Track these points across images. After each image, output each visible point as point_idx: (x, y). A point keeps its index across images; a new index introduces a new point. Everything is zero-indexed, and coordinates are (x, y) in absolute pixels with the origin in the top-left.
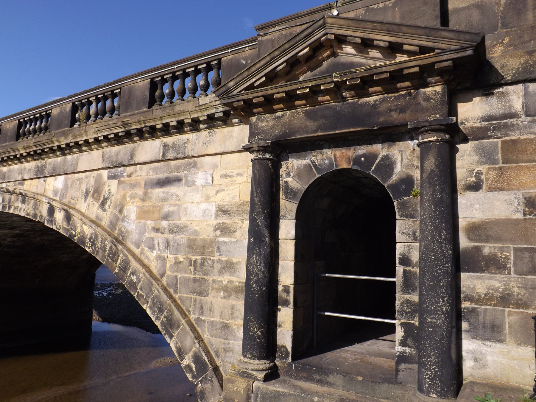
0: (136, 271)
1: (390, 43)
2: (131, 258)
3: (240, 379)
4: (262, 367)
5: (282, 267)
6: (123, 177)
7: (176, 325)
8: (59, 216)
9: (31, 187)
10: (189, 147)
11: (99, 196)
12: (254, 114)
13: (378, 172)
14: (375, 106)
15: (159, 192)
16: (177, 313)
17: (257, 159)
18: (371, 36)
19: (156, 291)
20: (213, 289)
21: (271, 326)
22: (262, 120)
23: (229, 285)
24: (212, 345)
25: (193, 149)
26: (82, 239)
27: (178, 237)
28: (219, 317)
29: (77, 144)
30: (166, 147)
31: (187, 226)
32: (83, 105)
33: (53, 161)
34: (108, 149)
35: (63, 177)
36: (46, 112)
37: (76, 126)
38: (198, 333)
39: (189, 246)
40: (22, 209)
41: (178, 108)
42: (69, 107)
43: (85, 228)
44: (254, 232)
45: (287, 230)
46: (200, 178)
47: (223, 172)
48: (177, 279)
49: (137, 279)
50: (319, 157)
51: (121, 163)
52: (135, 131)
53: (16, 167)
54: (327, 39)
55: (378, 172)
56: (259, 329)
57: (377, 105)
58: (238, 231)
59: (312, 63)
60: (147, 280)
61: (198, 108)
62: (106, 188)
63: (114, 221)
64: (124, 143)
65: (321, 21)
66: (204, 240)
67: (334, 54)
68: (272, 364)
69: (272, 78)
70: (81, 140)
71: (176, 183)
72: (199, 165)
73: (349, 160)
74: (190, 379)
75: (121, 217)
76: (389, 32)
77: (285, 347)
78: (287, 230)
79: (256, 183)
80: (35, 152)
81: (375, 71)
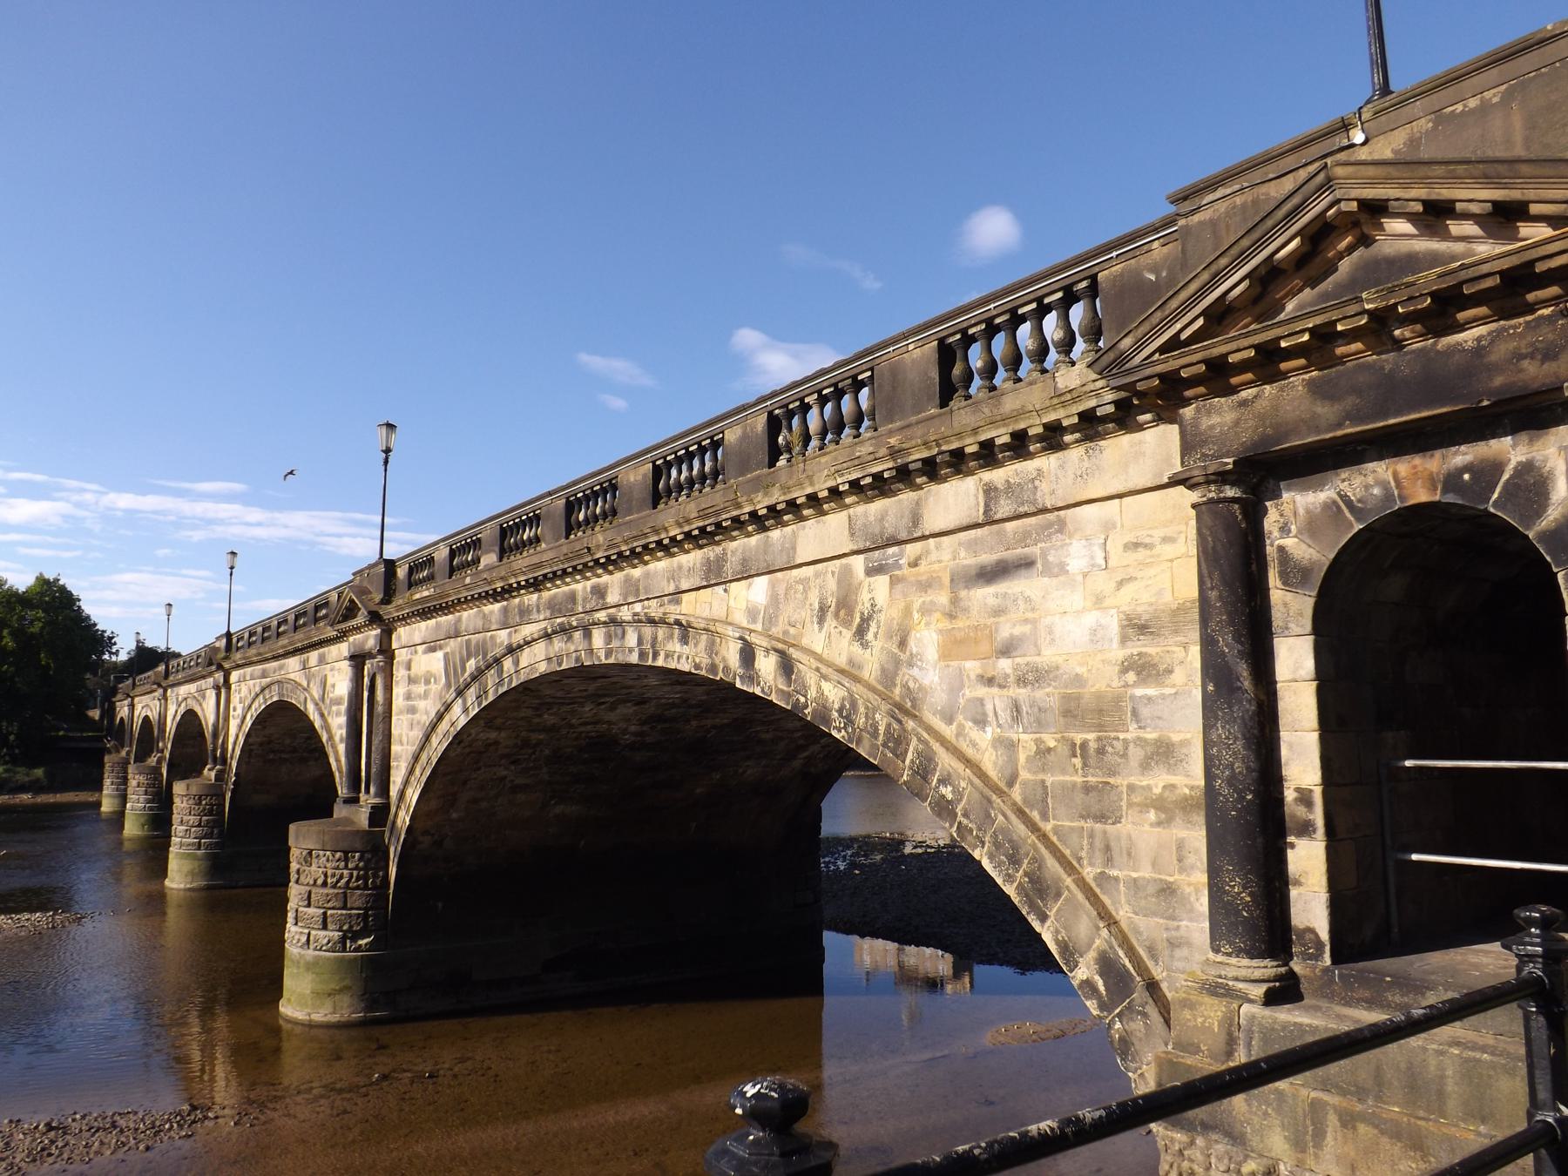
0: (949, 774)
1: (1495, 203)
2: (936, 746)
3: (1208, 1000)
4: (1258, 974)
5: (1291, 746)
6: (900, 567)
7: (1053, 892)
8: (766, 665)
9: (695, 607)
10: (1044, 487)
11: (850, 613)
12: (1186, 402)
13: (1509, 506)
14: (1479, 350)
15: (985, 594)
16: (1051, 863)
17: (1204, 503)
18: (1445, 193)
19: (1000, 817)
20: (1130, 805)
21: (1273, 884)
22: (1209, 413)
23: (1167, 794)
24: (1140, 933)
25: (1053, 492)
26: (823, 712)
27: (1039, 694)
28: (1150, 868)
29: (792, 506)
30: (990, 491)
31: (1057, 668)
32: (790, 414)
33: (740, 546)
34: (860, 509)
35: (765, 578)
36: (712, 438)
37: (782, 462)
38: (1104, 906)
39: (1067, 713)
40: (682, 657)
41: (1010, 404)
42: (760, 422)
43: (827, 687)
44: (1215, 669)
45: (1295, 659)
46: (1077, 555)
47: (1130, 538)
48: (1045, 788)
49: (953, 792)
50: (1358, 481)
51: (893, 537)
52: (919, 465)
53: (660, 565)
54: (1340, 213)
55: (1509, 506)
56: (1245, 888)
57: (1484, 347)
58: (1177, 670)
59: (1312, 269)
60: (976, 796)
61: (1056, 401)
62: (864, 597)
63: (890, 667)
64: (893, 493)
65: (1322, 176)
66: (1099, 696)
67: (1365, 241)
68: (1283, 970)
69: (1219, 317)
70: (800, 495)
71: (1023, 572)
72: (1070, 526)
73: (1432, 482)
74: (1095, 1013)
75: (903, 657)
76: (1488, 180)
77: (1312, 931)
78: (1295, 659)
79: (1208, 557)
80: (702, 530)
81: (1463, 275)
